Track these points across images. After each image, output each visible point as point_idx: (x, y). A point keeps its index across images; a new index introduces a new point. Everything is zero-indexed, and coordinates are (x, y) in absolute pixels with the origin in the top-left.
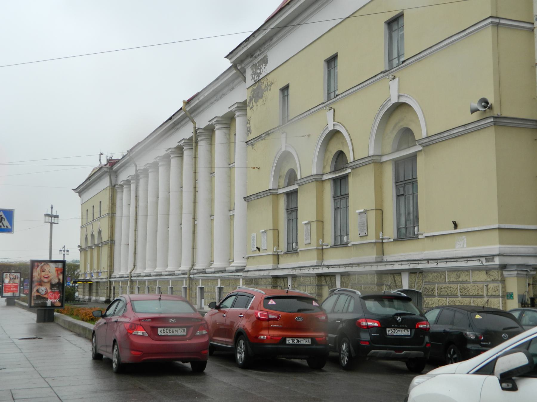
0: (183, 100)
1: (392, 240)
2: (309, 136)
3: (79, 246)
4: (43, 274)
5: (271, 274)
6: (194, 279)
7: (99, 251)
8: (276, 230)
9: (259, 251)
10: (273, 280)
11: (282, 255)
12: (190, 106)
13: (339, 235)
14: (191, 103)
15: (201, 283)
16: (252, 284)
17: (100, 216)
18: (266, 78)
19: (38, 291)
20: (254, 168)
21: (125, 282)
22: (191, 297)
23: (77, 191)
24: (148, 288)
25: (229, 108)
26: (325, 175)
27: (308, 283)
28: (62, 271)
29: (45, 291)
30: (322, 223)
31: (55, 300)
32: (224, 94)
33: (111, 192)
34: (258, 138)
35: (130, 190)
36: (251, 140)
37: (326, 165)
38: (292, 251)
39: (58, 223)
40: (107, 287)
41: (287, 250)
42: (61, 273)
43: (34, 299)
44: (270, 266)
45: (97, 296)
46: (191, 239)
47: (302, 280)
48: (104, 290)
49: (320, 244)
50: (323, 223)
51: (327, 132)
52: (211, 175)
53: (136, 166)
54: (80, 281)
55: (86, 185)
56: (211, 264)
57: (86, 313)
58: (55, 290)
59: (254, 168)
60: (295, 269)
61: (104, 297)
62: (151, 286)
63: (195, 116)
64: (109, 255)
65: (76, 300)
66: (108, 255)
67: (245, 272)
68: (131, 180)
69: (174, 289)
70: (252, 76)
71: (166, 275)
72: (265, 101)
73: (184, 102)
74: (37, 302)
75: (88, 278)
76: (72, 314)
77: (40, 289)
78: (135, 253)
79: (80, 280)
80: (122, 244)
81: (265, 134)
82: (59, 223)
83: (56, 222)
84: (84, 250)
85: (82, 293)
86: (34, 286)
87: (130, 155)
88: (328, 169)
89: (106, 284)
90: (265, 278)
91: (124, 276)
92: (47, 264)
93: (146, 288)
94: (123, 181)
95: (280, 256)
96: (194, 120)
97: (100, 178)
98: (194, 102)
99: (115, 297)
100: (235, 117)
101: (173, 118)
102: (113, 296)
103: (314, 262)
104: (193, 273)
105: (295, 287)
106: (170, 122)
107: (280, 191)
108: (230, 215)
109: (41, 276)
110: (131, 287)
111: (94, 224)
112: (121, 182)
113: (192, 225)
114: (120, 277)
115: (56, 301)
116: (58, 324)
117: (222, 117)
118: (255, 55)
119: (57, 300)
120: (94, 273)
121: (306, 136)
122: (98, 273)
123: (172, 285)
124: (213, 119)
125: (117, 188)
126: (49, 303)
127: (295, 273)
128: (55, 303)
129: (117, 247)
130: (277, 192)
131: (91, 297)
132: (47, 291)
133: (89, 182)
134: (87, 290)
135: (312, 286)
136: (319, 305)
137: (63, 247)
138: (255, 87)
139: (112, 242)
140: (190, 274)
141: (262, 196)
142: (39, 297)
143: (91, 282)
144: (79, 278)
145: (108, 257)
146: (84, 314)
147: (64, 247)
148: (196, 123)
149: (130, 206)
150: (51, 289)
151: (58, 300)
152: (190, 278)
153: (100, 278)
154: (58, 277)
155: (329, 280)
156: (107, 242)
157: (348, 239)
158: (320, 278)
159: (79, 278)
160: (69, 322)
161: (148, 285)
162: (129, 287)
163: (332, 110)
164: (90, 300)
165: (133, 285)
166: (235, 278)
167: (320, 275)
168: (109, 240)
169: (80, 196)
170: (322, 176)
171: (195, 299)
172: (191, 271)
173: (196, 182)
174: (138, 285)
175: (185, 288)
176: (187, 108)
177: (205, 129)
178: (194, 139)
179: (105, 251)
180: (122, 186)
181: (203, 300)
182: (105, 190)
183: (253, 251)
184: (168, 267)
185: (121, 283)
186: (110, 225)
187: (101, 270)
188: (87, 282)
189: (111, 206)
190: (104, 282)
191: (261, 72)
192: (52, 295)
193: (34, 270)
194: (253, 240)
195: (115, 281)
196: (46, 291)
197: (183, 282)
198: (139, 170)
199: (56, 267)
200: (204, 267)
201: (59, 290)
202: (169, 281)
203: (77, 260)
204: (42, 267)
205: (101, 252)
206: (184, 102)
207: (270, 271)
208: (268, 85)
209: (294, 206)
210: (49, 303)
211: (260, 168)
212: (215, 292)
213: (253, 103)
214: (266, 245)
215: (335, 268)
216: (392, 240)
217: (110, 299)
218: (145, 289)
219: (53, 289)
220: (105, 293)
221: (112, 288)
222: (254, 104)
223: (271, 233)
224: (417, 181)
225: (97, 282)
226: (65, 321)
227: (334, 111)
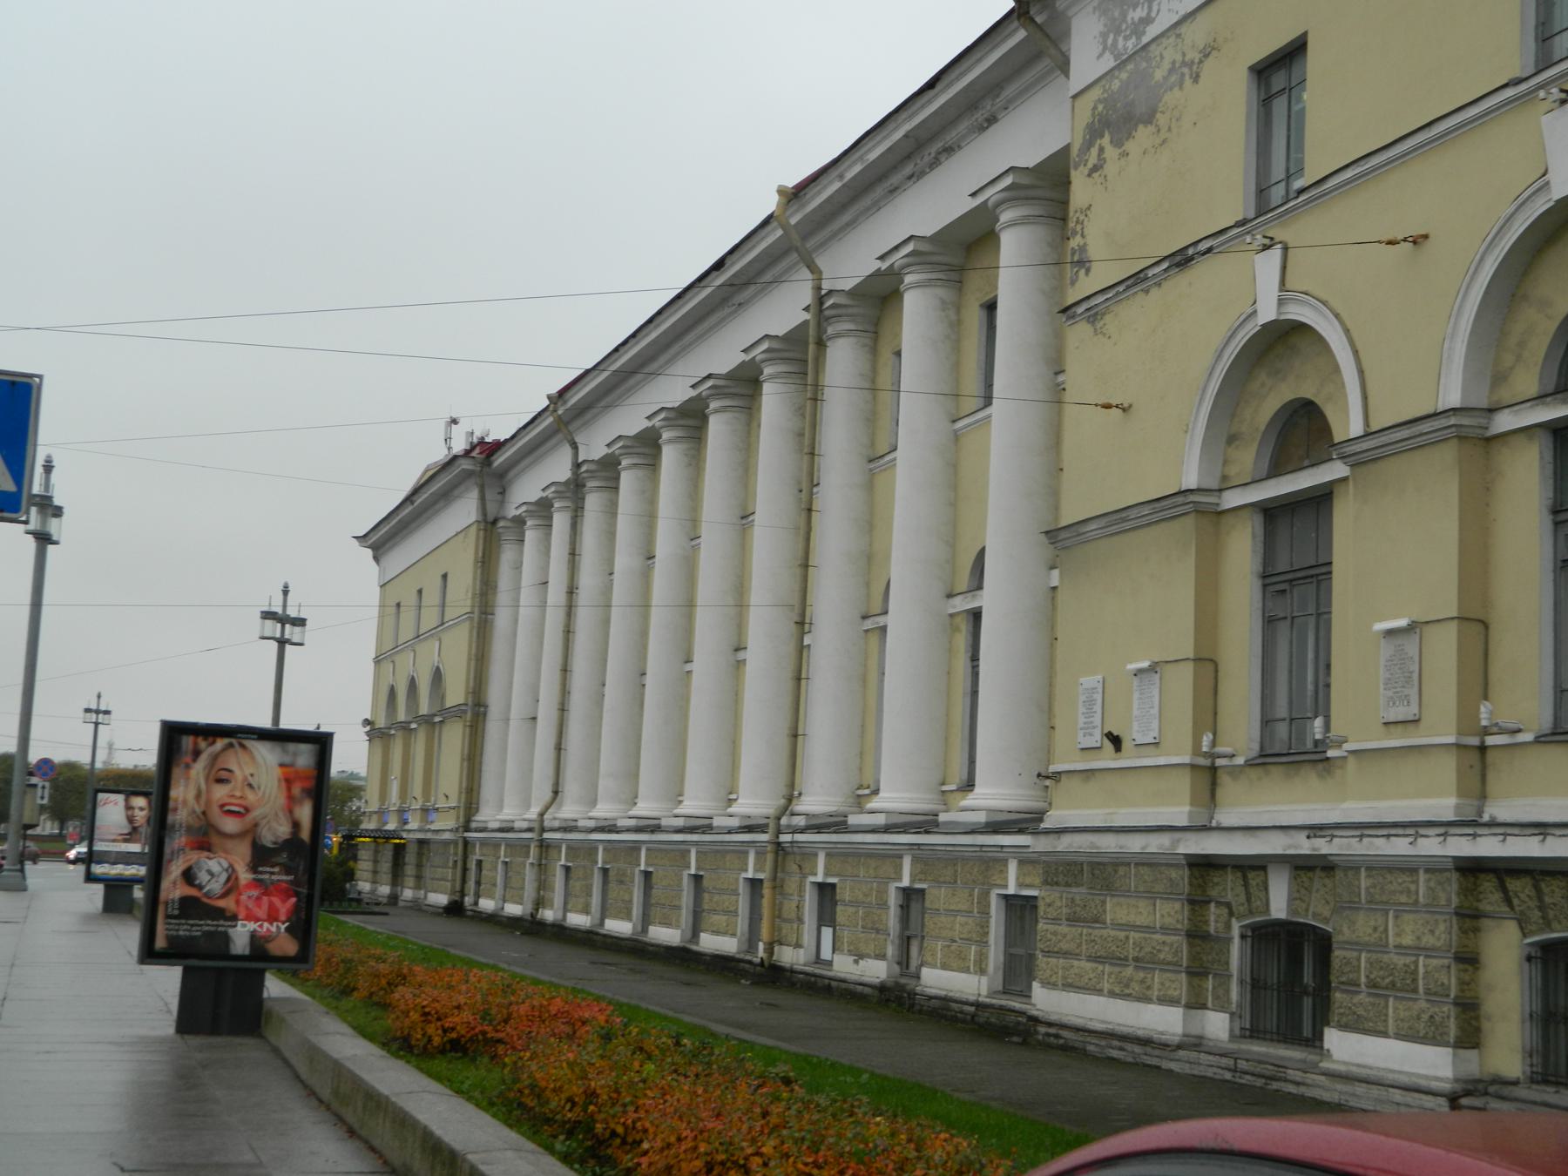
0: (780, 186)
2: (1418, 241)
3: (367, 722)
4: (220, 792)
5: (1182, 850)
6: (795, 849)
7: (433, 738)
8: (1207, 663)
10: (1192, 876)
11: (1235, 771)
12: (803, 206)
14: (808, 196)
15: (826, 867)
16: (1078, 885)
17: (443, 624)
18: (1179, 36)
19: (188, 876)
20: (1107, 406)
21: (521, 848)
22: (779, 917)
23: (370, 542)
24: (605, 871)
25: (973, 195)
26: (1507, 411)
27: (1403, 899)
28: (311, 784)
29: (224, 877)
30: (1479, 628)
31: (271, 924)
32: (949, 150)
33: (481, 542)
34: (1129, 282)
35: (549, 535)
36: (1088, 298)
37: (1512, 368)
39: (301, 644)
40: (456, 862)
41: (1262, 748)
42: (307, 792)
43: (168, 917)
45: (417, 887)
46: (787, 701)
47: (1364, 882)
48: (445, 870)
49: (1205, 749)
50: (1485, 625)
52: (872, 466)
53: (575, 446)
54: (365, 837)
55: (400, 521)
56: (730, 802)
57: (424, 1007)
58: (274, 877)
59: (1107, 406)
60: (1329, 832)
61: (441, 893)
62: (614, 864)
63: (823, 245)
64: (466, 752)
65: (352, 900)
67: (1048, 832)
68: (554, 498)
69: (705, 883)
70: (1104, 42)
71: (629, 830)
72: (1170, 129)
73: (781, 191)
74: (181, 933)
75: (391, 826)
76: (347, 986)
77: (200, 869)
78: (559, 748)
79: (367, 830)
80: (512, 716)
81: (1165, 265)
82: (305, 642)
83: (295, 640)
84: (383, 733)
85: (368, 875)
86: (173, 853)
87: (555, 411)
88: (1527, 381)
89: (452, 851)
90: (1147, 862)
91: (517, 825)
92: (243, 746)
93: (596, 871)
94: (524, 503)
95: (1219, 772)
96: (813, 262)
97: (446, 496)
98: (819, 193)
99: (479, 897)
100: (998, 227)
101: (728, 262)
102: (472, 892)
103: (1445, 806)
104: (789, 826)
105: (1307, 910)
106: (717, 277)
107: (1233, 499)
108: (952, 611)
109: (208, 802)
110: (540, 865)
111: (417, 648)
112: (517, 508)
113: (790, 648)
114: (501, 830)
115: (274, 929)
116: (276, 1051)
117: (936, 238)
119: (278, 927)
120: (410, 812)
121: (1405, 240)
122: (425, 811)
123: (698, 868)
124: (897, 248)
125: (500, 530)
126: (240, 936)
127: (1324, 852)
128: (268, 938)
129: (493, 727)
130: (1218, 504)
131: (399, 888)
132: (237, 879)
133: (408, 509)
134: (386, 866)
135: (1427, 916)
138: (1116, 81)
139: (476, 712)
141: (1145, 521)
142: (190, 907)
143: (402, 841)
144: (363, 826)
145: (463, 760)
146: (415, 1016)
148: (820, 272)
149: (547, 588)
150: (253, 868)
151: (283, 927)
152: (779, 844)
153: (433, 827)
154: (291, 812)
155: (1530, 890)
156: (463, 708)
157: (1327, 726)
158: (1472, 879)
159: (363, 826)
160: (338, 1070)
161: (604, 862)
162: (532, 864)
164: (394, 899)
165: (546, 858)
166: (983, 854)
167: (1471, 869)
168: (470, 703)
169: (376, 559)
170: (1220, 497)
171: (795, 926)
172: (784, 821)
173: (815, 490)
174: (567, 860)
175: (755, 884)
176: (792, 215)
177: (853, 293)
178: (812, 332)
179: (453, 738)
180: (519, 522)
181: (827, 933)
182: (461, 536)
183: (1083, 749)
184: (598, 807)
185: (503, 848)
186: (474, 651)
187: (436, 800)
188: (388, 838)
189: (481, 589)
190: (446, 843)
191: (1149, 14)
192: (258, 899)
193: (177, 772)
194: (1090, 703)
195: (484, 843)
196: (228, 880)
197: (747, 858)
198: (584, 461)
199: (282, 765)
200: (834, 809)
201: (291, 877)
202: (689, 851)
203: (352, 773)
204: (215, 758)
205: (440, 746)
206: (781, 191)
207: (1178, 835)
208: (1184, 64)
210: (240, 936)
211: (1130, 406)
212: (885, 903)
213: (1101, 150)
214: (1155, 724)
215: (1392, 839)
217: (462, 903)
218: (592, 874)
219: (266, 872)
220: (448, 881)
221: (472, 866)
222: (1111, 152)
223: (1183, 680)
224: (1330, 573)
225: (421, 842)
226: (315, 1054)
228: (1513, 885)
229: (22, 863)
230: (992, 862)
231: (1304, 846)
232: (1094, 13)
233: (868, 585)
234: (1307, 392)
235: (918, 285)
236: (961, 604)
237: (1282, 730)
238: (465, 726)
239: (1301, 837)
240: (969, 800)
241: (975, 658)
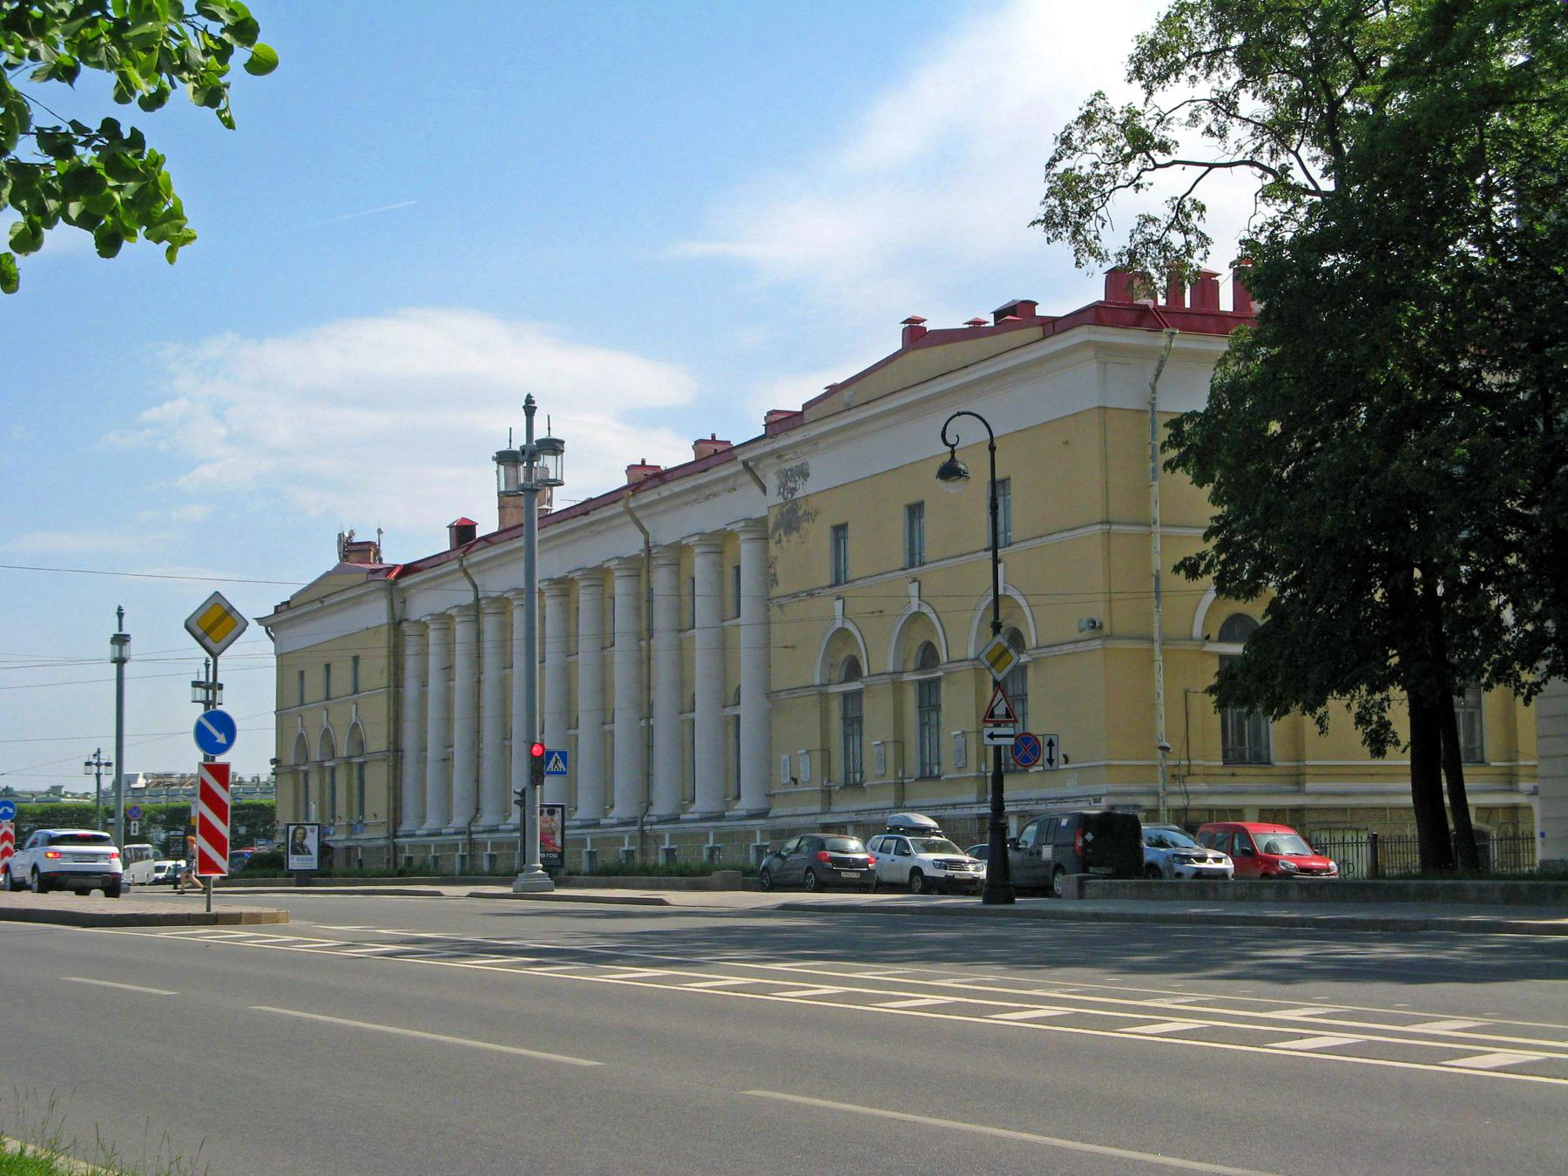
5: (819, 822)
8: (826, 752)
9: (796, 783)
13: (212, 906)
20: (786, 647)
38: (853, 785)
44: (817, 808)
59: (786, 647)
66: (388, 786)
88: (911, 665)
118: (786, 457)
136: (550, 519)
137: (95, 751)
140: (643, 825)
147: (99, 752)
163: (916, 584)
194: (785, 766)
209: (858, 714)
222: (784, 538)
223: (817, 756)
227: (920, 585)
230: (750, 835)
231: (854, 817)
232: (1165, 470)
233: (681, 697)
236: (730, 711)
238: (389, 766)
240: (739, 805)
241: (738, 737)
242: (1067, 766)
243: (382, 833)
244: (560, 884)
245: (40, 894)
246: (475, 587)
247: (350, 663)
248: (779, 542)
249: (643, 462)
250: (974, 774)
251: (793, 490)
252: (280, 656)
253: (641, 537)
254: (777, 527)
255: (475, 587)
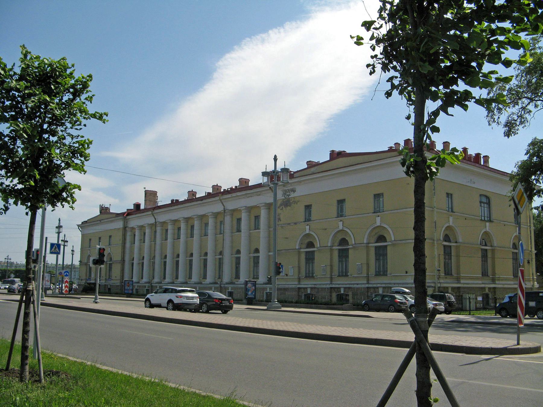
1: (303, 277)
51: (304, 234)
88: (336, 244)
140: (221, 284)
163: (309, 226)
167: (331, 288)
177: (131, 228)
216: (303, 277)
228: (335, 289)
229: (28, 270)
234: (311, 240)
235: (263, 209)
237: (340, 273)
239: (313, 285)
242: (407, 274)
243: (119, 282)
244: (283, 306)
245: (150, 309)
246: (155, 219)
247: (108, 237)
248: (282, 209)
249: (192, 190)
250: (366, 275)
251: (289, 195)
252: (83, 236)
253: (223, 207)
254: (281, 205)
255: (155, 219)
